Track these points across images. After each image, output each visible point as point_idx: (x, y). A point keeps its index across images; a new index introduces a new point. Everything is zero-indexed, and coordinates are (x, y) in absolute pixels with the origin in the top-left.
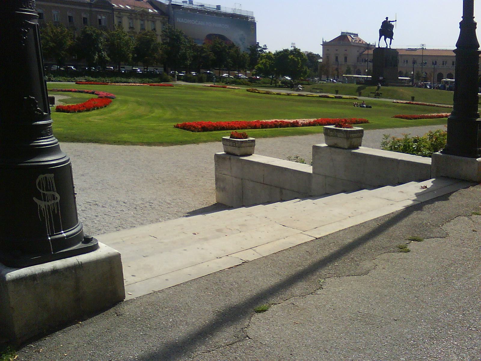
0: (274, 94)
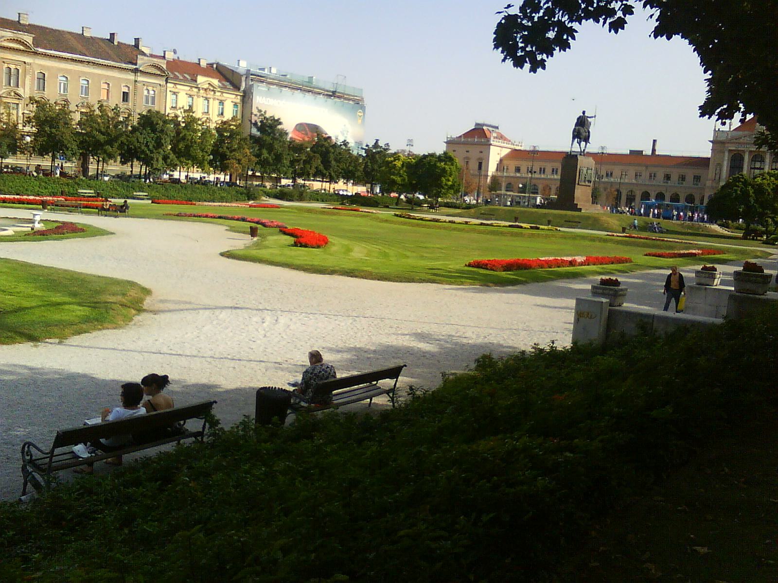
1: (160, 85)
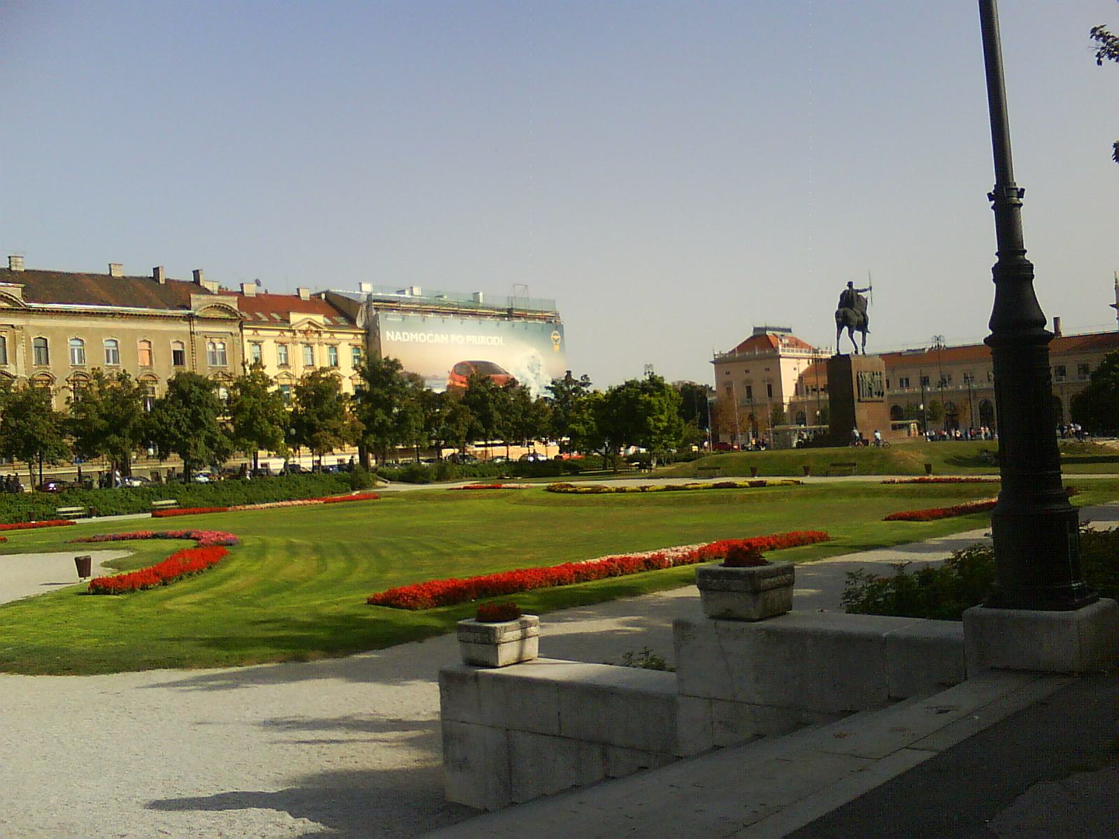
0: (610, 492)
1: (231, 334)
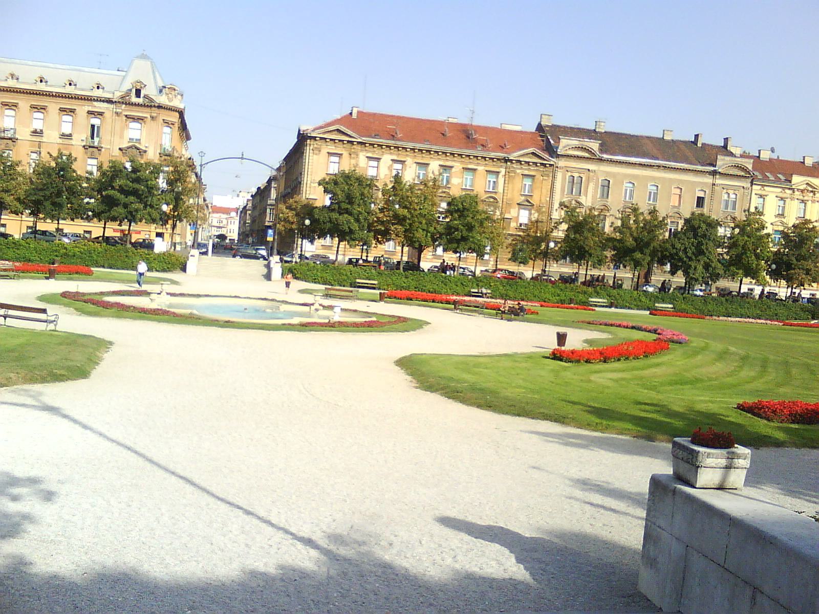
1: (743, 187)
